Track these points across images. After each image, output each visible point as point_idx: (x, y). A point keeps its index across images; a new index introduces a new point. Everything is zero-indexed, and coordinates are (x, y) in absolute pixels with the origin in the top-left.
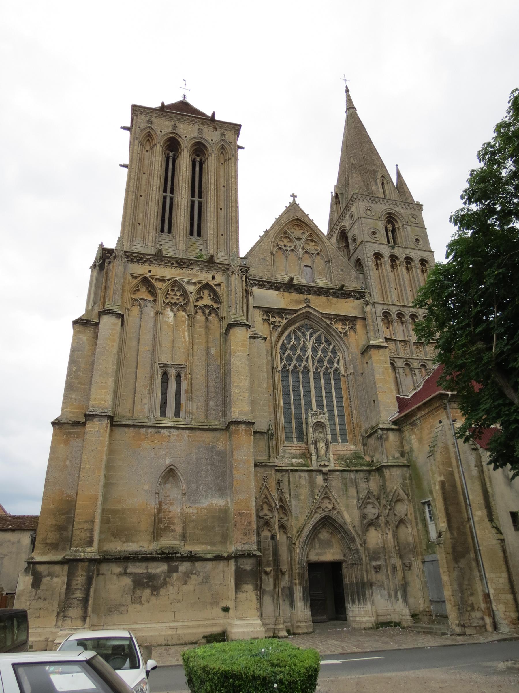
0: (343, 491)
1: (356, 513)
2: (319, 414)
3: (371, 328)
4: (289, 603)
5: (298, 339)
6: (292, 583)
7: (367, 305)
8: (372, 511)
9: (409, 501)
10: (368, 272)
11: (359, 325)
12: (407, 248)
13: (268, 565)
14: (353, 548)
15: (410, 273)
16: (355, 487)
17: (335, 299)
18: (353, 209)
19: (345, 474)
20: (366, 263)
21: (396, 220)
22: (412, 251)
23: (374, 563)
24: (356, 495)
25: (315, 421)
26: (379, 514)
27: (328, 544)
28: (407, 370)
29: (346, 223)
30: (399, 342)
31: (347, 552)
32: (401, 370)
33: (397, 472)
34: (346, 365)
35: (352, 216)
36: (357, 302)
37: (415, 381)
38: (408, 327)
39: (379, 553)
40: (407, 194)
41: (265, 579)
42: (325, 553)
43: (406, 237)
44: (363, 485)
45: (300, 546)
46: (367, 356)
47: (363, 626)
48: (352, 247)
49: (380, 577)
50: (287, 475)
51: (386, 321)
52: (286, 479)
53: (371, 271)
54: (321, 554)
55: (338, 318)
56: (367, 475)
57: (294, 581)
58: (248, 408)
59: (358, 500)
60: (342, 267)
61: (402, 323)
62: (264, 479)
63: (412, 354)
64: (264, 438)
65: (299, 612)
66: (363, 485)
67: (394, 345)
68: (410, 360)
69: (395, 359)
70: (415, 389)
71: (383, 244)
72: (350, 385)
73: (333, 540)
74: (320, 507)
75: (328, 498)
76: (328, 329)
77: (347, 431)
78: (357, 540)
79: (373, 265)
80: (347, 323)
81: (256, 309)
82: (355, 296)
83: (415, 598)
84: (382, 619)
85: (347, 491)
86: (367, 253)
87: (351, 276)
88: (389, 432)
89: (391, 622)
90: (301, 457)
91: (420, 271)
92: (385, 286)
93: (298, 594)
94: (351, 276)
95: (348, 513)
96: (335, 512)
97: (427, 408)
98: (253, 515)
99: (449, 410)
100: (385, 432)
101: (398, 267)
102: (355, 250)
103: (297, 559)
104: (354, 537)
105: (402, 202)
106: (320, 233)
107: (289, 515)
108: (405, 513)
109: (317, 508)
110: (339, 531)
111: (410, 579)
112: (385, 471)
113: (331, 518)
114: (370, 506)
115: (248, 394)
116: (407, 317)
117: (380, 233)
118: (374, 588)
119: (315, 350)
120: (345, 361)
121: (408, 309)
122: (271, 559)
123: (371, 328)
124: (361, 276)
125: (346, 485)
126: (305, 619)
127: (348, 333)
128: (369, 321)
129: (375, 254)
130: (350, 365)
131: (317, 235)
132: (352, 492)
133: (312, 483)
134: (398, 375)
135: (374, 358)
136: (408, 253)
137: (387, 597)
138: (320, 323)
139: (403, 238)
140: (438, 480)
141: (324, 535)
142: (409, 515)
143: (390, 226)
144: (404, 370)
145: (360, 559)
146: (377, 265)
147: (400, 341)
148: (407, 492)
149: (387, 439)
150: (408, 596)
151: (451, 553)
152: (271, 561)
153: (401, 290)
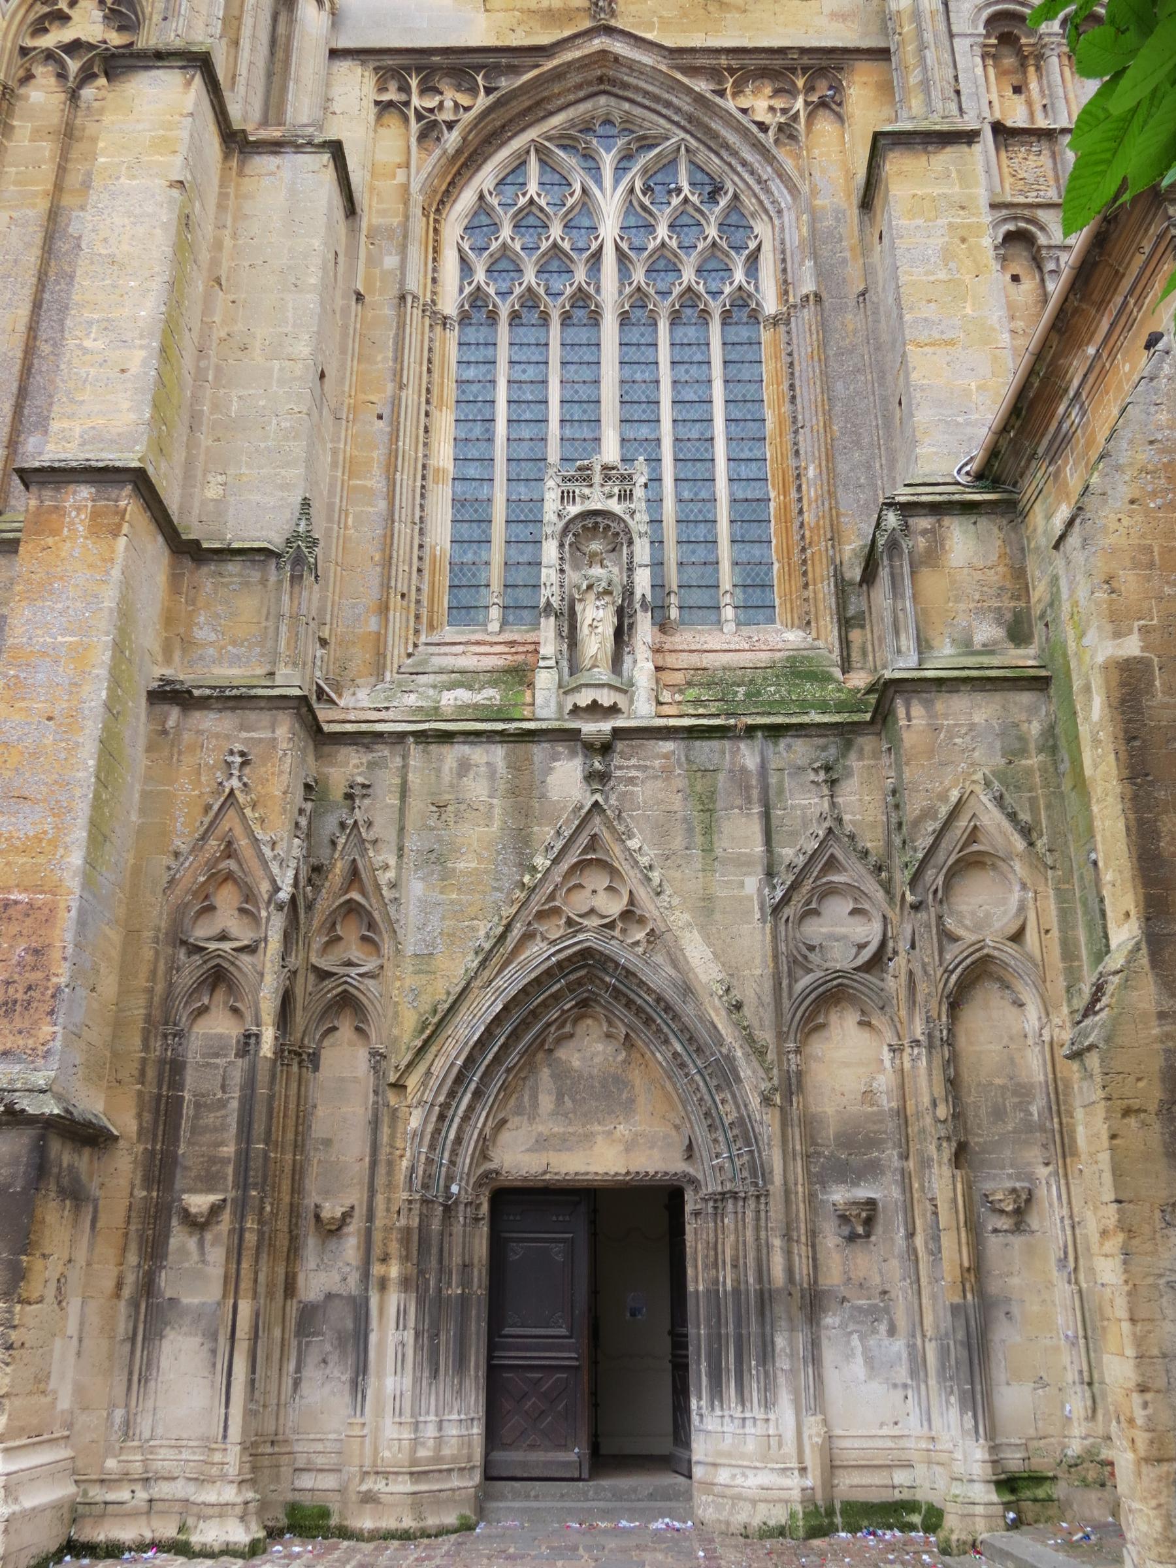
0: (690, 830)
1: (753, 941)
2: (597, 479)
4: (346, 1377)
5: (558, 180)
6: (366, 1275)
8: (842, 932)
9: (1038, 864)
13: (208, 1183)
14: (729, 1112)
16: (757, 809)
19: (706, 749)
23: (839, 1195)
24: (759, 849)
25: (573, 510)
26: (883, 944)
27: (610, 1096)
31: (701, 1134)
33: (981, 711)
34: (784, 270)
39: (873, 1143)
41: (183, 1250)
42: (589, 1137)
44: (804, 803)
45: (428, 1096)
47: (743, 1516)
49: (879, 1264)
50: (398, 761)
51: (1009, 61)
52: (388, 779)
54: (563, 1143)
55: (751, 63)
56: (833, 750)
57: (377, 1269)
58: (132, 416)
59: (770, 874)
62: (229, 765)
64: (264, 582)
65: (388, 1420)
66: (804, 803)
67: (1045, 159)
73: (636, 1077)
74: (556, 911)
75: (604, 865)
76: (701, 122)
77: (776, 566)
78: (748, 1071)
80: (800, 83)
81: (344, 66)
83: (1040, 1382)
84: (854, 1485)
85: (708, 831)
88: (947, 521)
89: (911, 1506)
90: (494, 684)
93: (392, 1332)
95: (707, 938)
96: (640, 935)
97: (1101, 305)
98: (62, 914)
100: (923, 523)
103: (405, 1163)
104: (730, 1059)
107: (387, 947)
108: (1013, 928)
109: (541, 915)
110: (659, 1030)
111: (1015, 1281)
112: (901, 712)
113: (617, 964)
114: (838, 908)
115: (143, 353)
118: (831, 1320)
119: (638, 220)
122: (229, 1150)
125: (707, 805)
126: (414, 1462)
127: (802, 125)
130: (802, 264)
132: (742, 833)
133: (524, 795)
137: (902, 1373)
138: (668, 104)
140: (1100, 659)
141: (590, 1050)
142: (1031, 936)
145: (758, 1171)
148: (1025, 817)
149: (933, 555)
150: (999, 1373)
151: (1153, 1107)
152: (225, 1161)
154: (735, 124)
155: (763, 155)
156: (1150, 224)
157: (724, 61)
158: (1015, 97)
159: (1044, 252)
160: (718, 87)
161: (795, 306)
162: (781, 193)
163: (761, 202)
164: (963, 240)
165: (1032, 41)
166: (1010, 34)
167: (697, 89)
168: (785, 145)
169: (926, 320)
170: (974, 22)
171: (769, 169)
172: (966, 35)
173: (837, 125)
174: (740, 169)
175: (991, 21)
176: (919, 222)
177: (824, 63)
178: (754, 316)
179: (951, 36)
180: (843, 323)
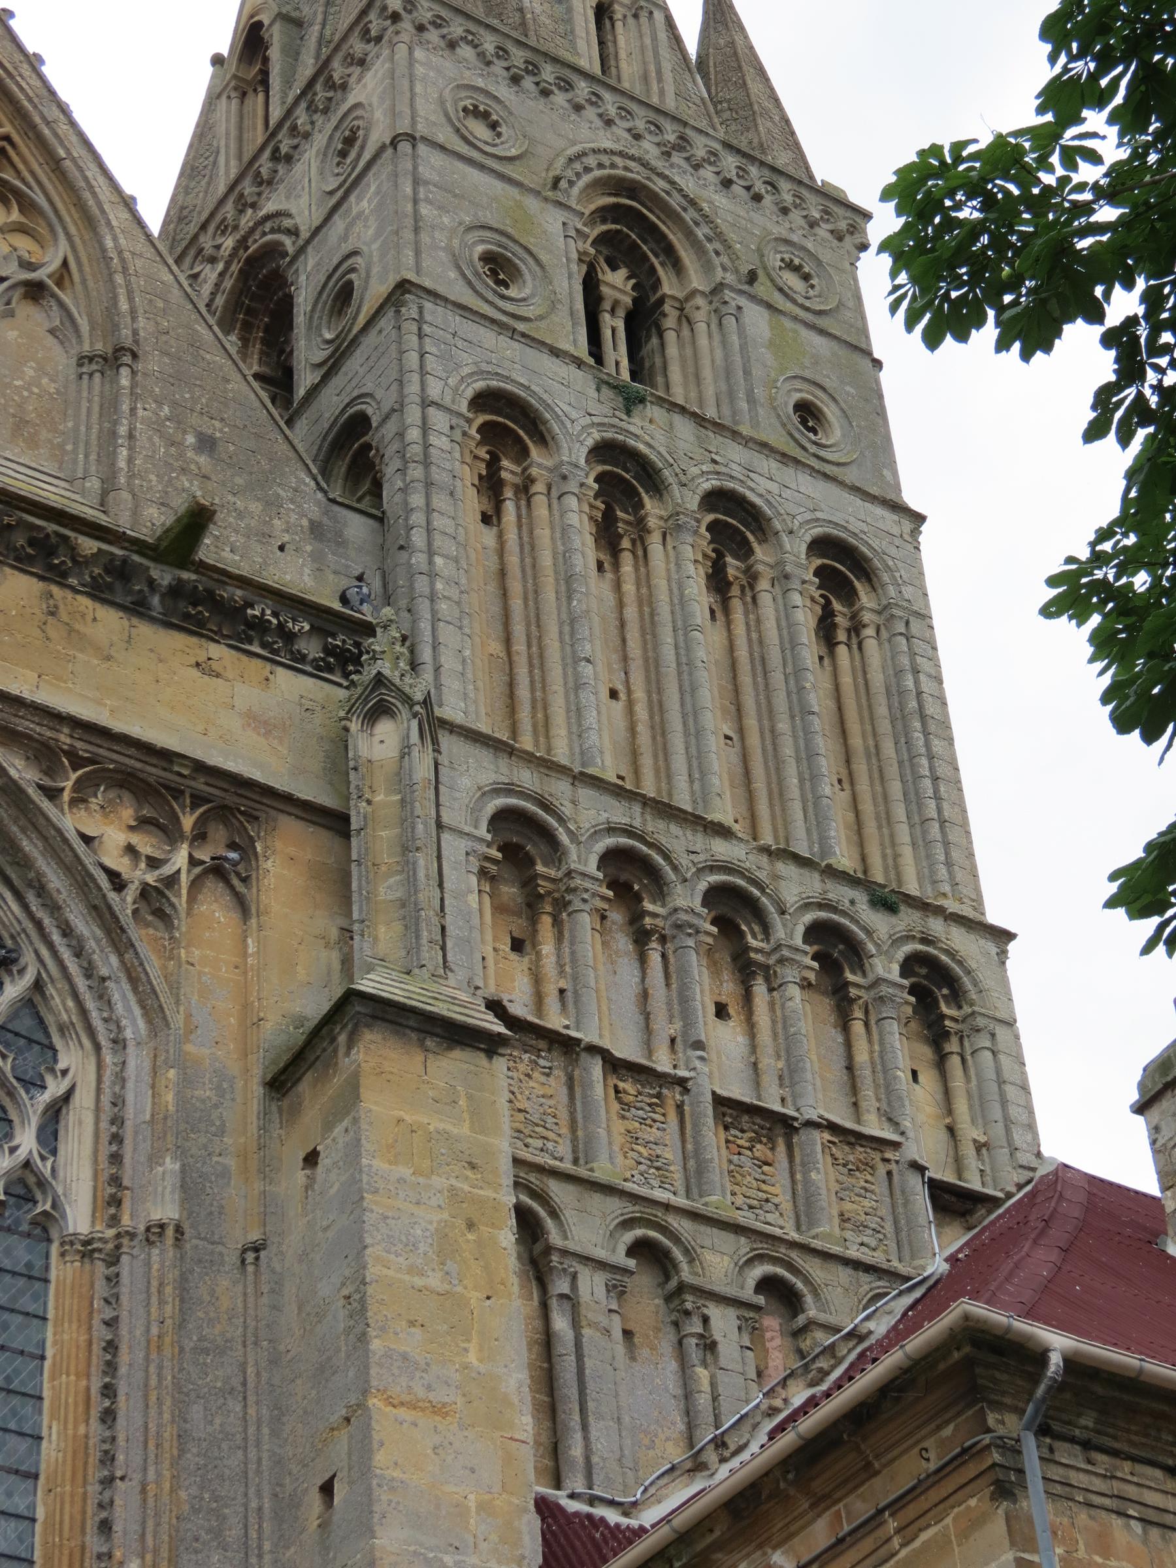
3: (388, 890)
7: (378, 711)
10: (417, 500)
11: (285, 861)
12: (735, 435)
15: (738, 615)
17: (108, 622)
18: (367, 89)
20: (414, 434)
21: (669, 252)
22: (770, 465)
28: (646, 1304)
29: (299, 196)
30: (596, 1068)
32: (592, 1287)
34: (116, 1159)
35: (349, 141)
36: (291, 686)
37: (703, 1400)
38: (684, 971)
40: (763, 125)
43: (728, 373)
46: (314, 1096)
48: (308, 350)
51: (510, 891)
53: (440, 501)
55: (113, 758)
60: (216, 429)
61: (641, 938)
63: (696, 1179)
67: (556, 1085)
68: (674, 1222)
69: (557, 1190)
70: (698, 1466)
71: (555, 352)
72: (131, 1333)
79: (468, 476)
80: (188, 822)
82: (289, 637)
86: (430, 380)
87: (273, 505)
91: (812, 623)
92: (536, 641)
94: (273, 505)
97: (822, 1502)
99: (1036, 1501)
101: (654, 542)
102: (331, 367)
105: (727, 146)
106: (78, 151)
116: (688, 898)
117: (547, 278)
120: (117, 1120)
121: (698, 841)
123: (388, 890)
124: (356, 527)
127: (181, 900)
128: (378, 839)
129: (484, 400)
130: (154, 1159)
131: (56, 165)
134: (561, 1323)
135: (377, 1104)
136: (736, 471)
139: (707, 373)
143: (617, 283)
144: (618, 1291)
146: (491, 485)
147: (614, 1065)
153: (658, 708)
154: (69, 859)
155: (108, 932)
156: (948, 1422)
157: (64, 738)
158: (513, 956)
159: (555, 1258)
160: (47, 782)
161: (132, 1236)
162: (129, 1009)
163: (83, 1012)
164: (471, 1225)
165: (552, 873)
166: (519, 847)
167: (13, 773)
168: (148, 925)
169: (405, 1357)
170: (475, 810)
171: (114, 960)
172: (461, 833)
173: (235, 916)
174: (56, 937)
175: (501, 818)
176: (405, 1171)
177: (231, 800)
178: (44, 1227)
179: (440, 826)
180: (212, 1293)
